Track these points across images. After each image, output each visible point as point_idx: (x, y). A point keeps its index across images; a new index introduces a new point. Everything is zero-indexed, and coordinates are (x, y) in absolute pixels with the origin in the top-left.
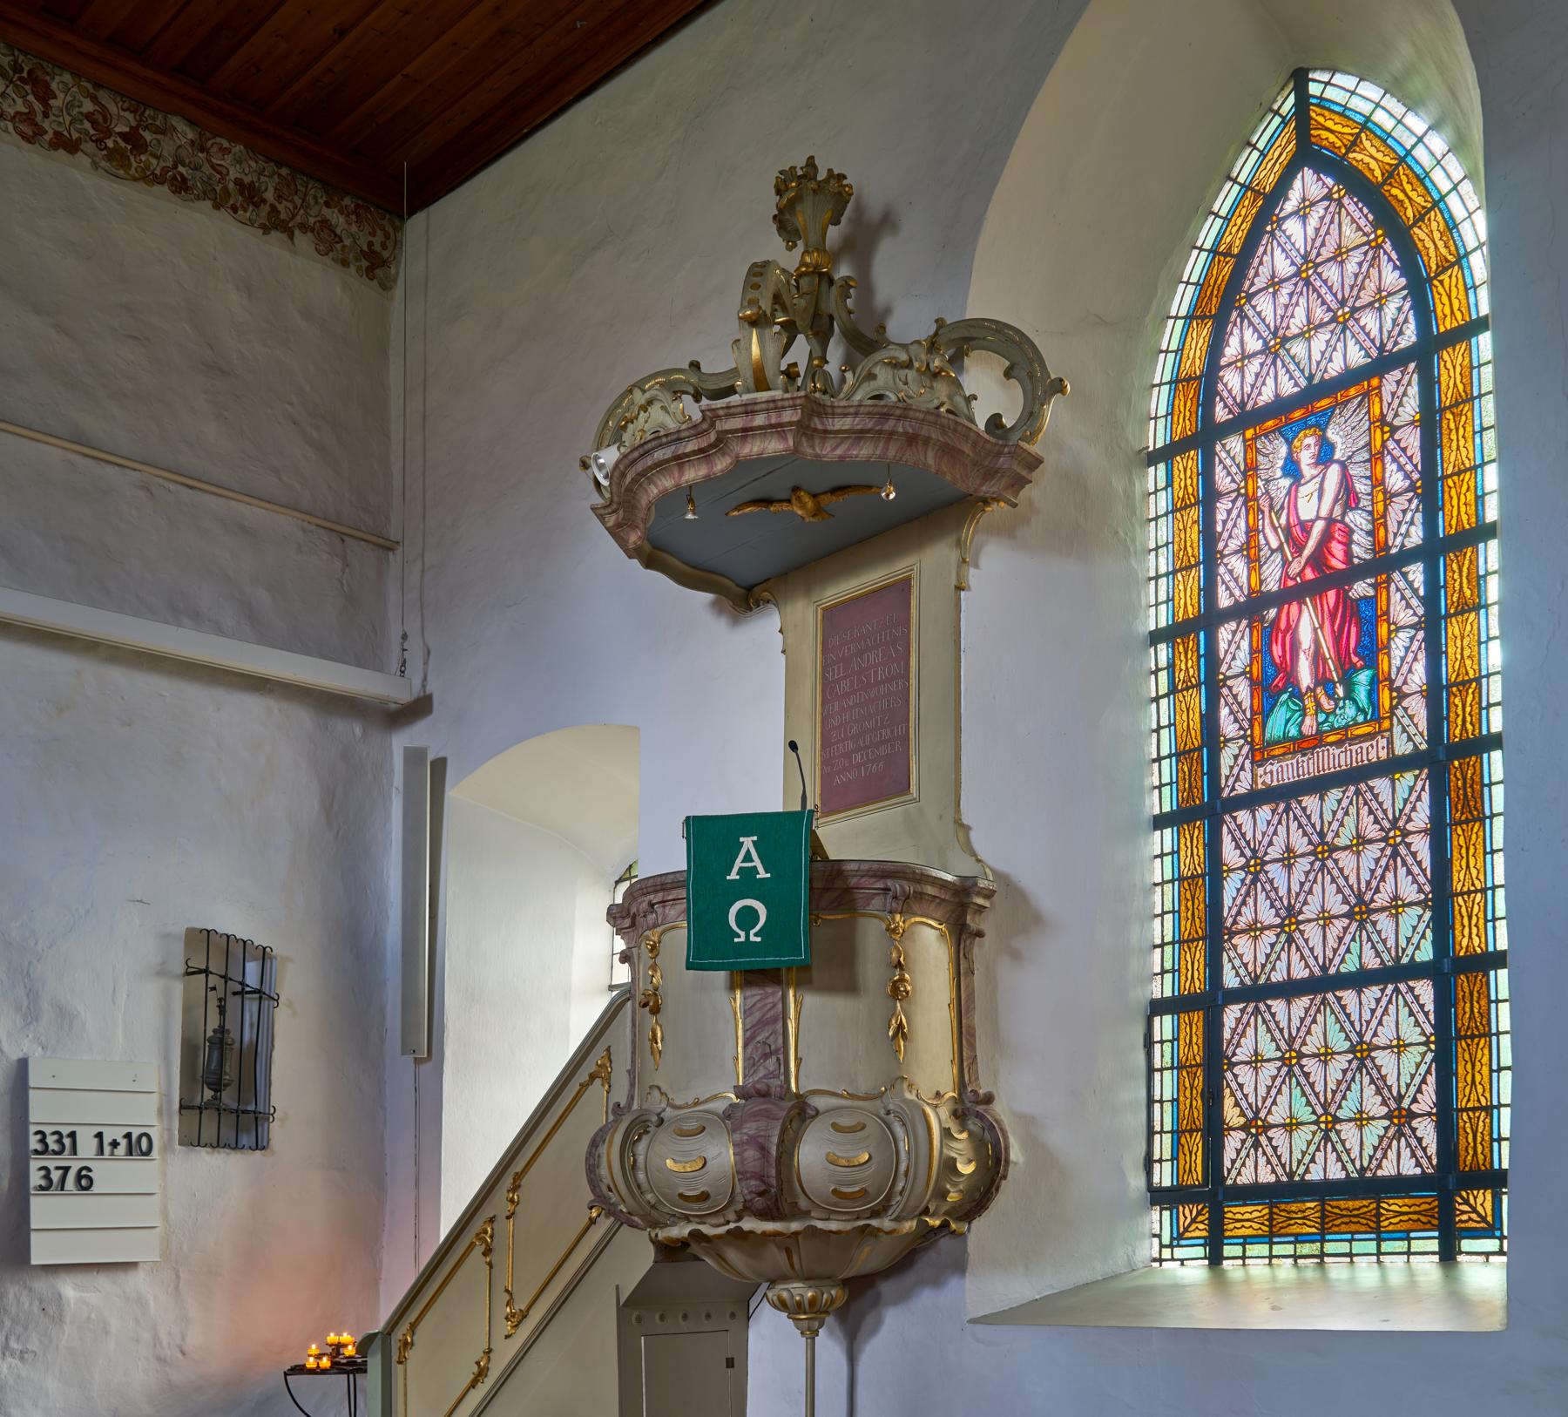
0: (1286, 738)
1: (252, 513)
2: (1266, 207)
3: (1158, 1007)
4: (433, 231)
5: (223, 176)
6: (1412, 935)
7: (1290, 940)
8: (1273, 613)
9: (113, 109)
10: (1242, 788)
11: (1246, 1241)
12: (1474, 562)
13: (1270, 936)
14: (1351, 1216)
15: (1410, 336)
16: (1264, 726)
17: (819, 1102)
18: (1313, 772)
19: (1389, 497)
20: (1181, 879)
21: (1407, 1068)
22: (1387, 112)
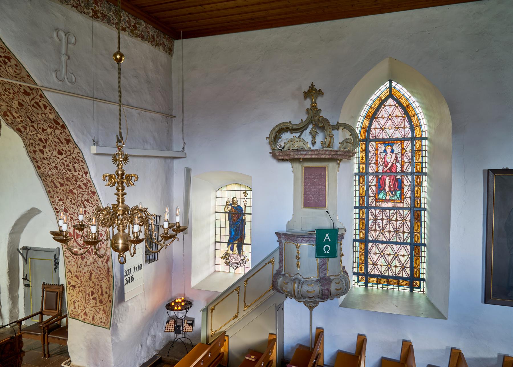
0: (382, 199)
1: (154, 115)
2: (382, 103)
3: (355, 240)
4: (185, 46)
5: (149, 34)
6: (406, 237)
7: (382, 234)
8: (380, 176)
9: (131, 19)
10: (374, 205)
11: (372, 284)
12: (420, 178)
13: (378, 232)
14: (393, 282)
15: (410, 136)
16: (378, 196)
17: (332, 278)
18: (388, 206)
19: (405, 163)
20: (360, 219)
21: (405, 259)
22: (404, 90)
